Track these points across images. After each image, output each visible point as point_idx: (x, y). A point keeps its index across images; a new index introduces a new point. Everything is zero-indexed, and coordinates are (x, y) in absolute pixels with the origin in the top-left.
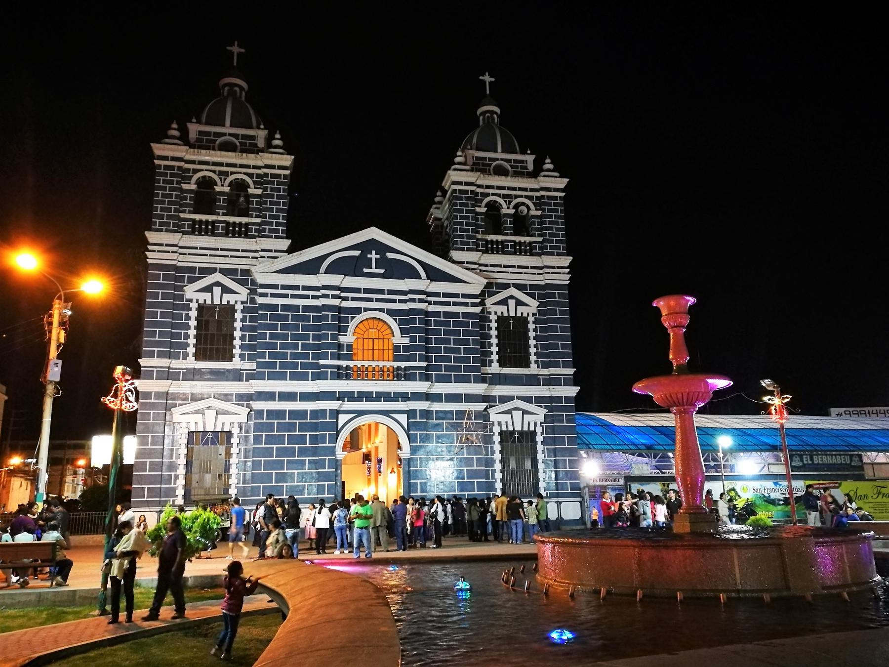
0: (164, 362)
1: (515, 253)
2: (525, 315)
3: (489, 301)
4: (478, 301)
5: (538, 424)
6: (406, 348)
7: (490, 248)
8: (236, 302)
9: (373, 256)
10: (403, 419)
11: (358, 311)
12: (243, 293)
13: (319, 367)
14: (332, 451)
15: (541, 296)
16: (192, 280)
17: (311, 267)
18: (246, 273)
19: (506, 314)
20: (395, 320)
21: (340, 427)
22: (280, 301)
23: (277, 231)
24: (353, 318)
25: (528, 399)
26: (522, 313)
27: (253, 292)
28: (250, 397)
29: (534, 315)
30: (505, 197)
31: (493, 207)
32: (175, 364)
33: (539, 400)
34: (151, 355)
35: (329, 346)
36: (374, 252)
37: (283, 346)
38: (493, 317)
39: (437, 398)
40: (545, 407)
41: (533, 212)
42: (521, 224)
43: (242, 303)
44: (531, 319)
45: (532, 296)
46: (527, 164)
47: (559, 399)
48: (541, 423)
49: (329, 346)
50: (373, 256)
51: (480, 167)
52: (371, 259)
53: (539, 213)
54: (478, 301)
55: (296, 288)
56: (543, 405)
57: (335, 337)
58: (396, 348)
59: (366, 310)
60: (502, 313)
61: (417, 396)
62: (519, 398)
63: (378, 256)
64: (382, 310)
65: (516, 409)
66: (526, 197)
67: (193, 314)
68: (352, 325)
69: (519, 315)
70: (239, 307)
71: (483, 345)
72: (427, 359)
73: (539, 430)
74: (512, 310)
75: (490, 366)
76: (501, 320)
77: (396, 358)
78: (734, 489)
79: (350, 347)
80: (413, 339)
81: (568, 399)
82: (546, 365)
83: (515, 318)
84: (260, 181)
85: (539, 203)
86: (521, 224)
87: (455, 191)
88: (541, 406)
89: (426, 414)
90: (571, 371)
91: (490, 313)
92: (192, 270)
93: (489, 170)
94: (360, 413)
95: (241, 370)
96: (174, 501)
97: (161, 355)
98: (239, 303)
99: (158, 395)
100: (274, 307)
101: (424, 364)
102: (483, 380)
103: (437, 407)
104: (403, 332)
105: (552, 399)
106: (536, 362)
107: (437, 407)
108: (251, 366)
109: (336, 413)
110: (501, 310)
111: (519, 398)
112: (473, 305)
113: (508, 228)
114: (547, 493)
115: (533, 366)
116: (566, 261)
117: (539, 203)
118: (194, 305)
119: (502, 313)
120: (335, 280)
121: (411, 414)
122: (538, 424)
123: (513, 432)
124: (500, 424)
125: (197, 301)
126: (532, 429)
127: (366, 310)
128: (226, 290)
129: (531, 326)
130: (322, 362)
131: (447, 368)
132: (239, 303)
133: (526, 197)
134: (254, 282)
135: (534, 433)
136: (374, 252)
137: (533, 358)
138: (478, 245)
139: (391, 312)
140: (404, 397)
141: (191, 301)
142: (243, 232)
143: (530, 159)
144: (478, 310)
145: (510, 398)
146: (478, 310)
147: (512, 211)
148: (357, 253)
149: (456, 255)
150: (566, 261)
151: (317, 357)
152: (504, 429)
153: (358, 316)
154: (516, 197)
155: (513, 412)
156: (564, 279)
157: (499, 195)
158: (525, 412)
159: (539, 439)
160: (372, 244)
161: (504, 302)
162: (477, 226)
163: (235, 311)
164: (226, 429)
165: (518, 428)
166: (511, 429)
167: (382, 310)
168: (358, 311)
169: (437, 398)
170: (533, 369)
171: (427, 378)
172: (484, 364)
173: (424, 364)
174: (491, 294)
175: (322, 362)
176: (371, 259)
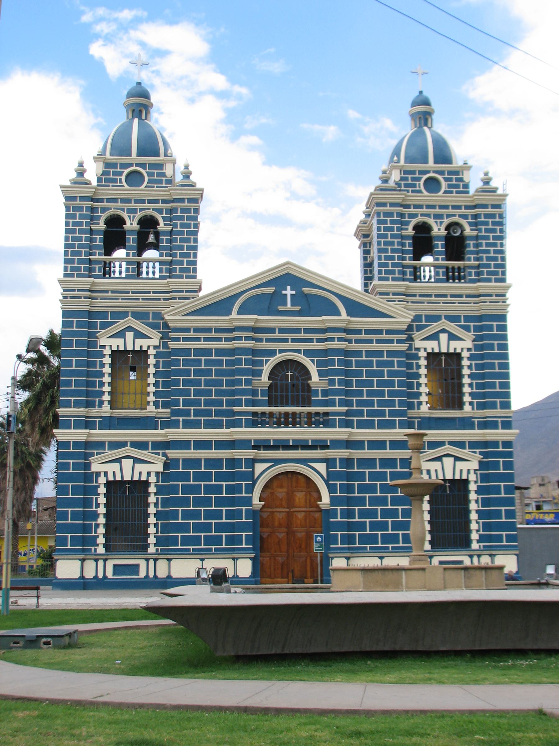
0: (82, 411)
1: (447, 280)
2: (458, 351)
4: (404, 337)
5: (472, 472)
8: (149, 347)
9: (289, 292)
10: (322, 468)
11: (272, 353)
13: (234, 413)
14: (248, 501)
15: (476, 329)
16: (105, 326)
18: (158, 315)
19: (437, 351)
20: (313, 361)
21: (256, 476)
22: (213, 345)
23: (393, 272)
24: (267, 361)
25: (460, 444)
26: (455, 349)
27: (165, 336)
28: (159, 446)
30: (437, 216)
32: (94, 412)
33: (474, 445)
34: (67, 404)
35: (243, 392)
36: (289, 288)
37: (218, 393)
40: (480, 453)
43: (155, 347)
45: (467, 328)
46: (462, 175)
47: (495, 444)
48: (475, 470)
49: (243, 392)
50: (289, 292)
52: (286, 295)
54: (404, 337)
55: (297, 331)
56: (161, 451)
57: (248, 382)
59: (281, 351)
60: (433, 349)
61: (337, 444)
62: (451, 443)
63: (294, 292)
64: (298, 351)
65: (448, 455)
66: (461, 216)
69: (451, 351)
71: (410, 386)
72: (348, 403)
73: (472, 477)
75: (419, 408)
76: (432, 357)
80: (332, 382)
82: (482, 406)
83: (448, 355)
88: (475, 452)
89: (348, 462)
92: (103, 315)
93: (121, 179)
94: (277, 462)
95: (156, 418)
96: (95, 550)
97: (77, 404)
98: (152, 348)
99: (77, 444)
102: (410, 425)
103: (357, 454)
105: (485, 444)
106: (471, 403)
107: (357, 454)
108: (164, 412)
109: (252, 462)
111: (451, 443)
112: (399, 341)
114: (480, 546)
115: (467, 408)
118: (422, 354)
119: (433, 349)
120: (250, 319)
121: (330, 462)
122: (472, 472)
123: (123, 482)
124: (106, 473)
125: (111, 346)
126: (464, 477)
127: (281, 351)
129: (152, 361)
130: (236, 409)
132: (152, 348)
133: (461, 216)
134: (166, 326)
135: (466, 482)
136: (289, 288)
137: (467, 399)
138: (404, 273)
139: (308, 353)
145: (441, 444)
146: (403, 347)
148: (271, 289)
151: (230, 403)
152: (111, 478)
153: (272, 359)
154: (448, 216)
155: (444, 459)
157: (428, 215)
158: (457, 459)
159: (472, 487)
161: (434, 337)
162: (403, 252)
163: (148, 356)
164: (144, 478)
165: (127, 478)
166: (119, 478)
167: (298, 351)
168: (272, 353)
171: (348, 424)
172: (411, 406)
174: (420, 328)
175: (236, 409)
176: (286, 295)
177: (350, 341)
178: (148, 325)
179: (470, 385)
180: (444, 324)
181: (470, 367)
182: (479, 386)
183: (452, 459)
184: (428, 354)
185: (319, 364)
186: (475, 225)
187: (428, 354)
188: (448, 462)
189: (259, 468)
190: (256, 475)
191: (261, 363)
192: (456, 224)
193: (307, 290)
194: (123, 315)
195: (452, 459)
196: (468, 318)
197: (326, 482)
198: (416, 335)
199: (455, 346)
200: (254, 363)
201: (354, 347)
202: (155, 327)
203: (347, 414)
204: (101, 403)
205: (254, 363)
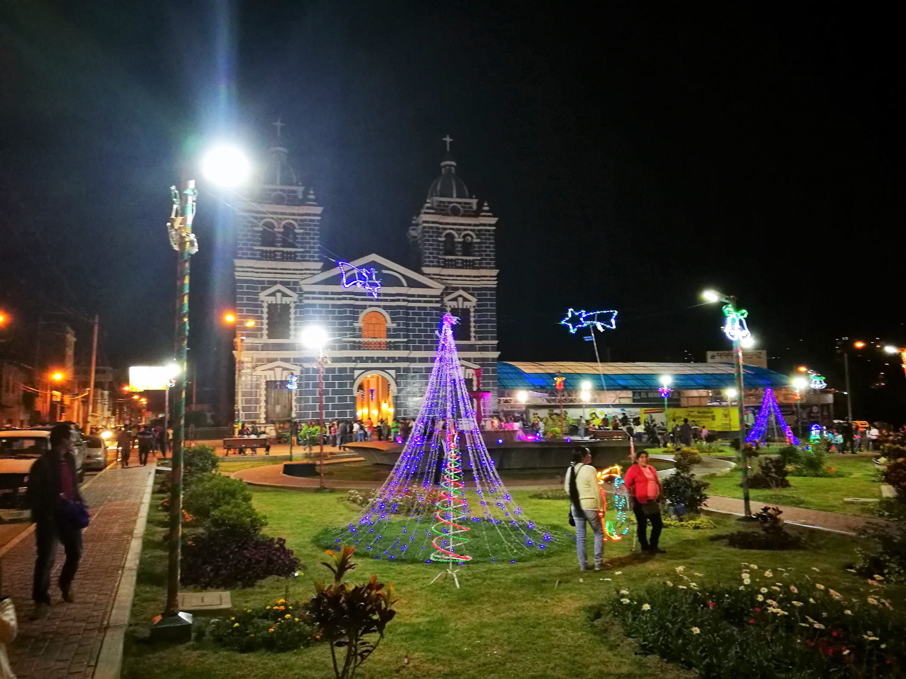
3: (446, 299)
6: (395, 330)
7: (448, 264)
10: (393, 372)
11: (365, 307)
12: (295, 296)
16: (264, 289)
17: (336, 280)
19: (274, 302)
29: (295, 302)
31: (450, 237)
38: (449, 309)
39: (413, 360)
41: (475, 240)
42: (467, 248)
44: (472, 310)
47: (487, 359)
51: (441, 210)
53: (478, 240)
58: (388, 330)
61: (401, 360)
64: (379, 306)
65: (277, 367)
67: (265, 310)
68: (361, 316)
69: (284, 303)
70: (292, 305)
72: (406, 336)
74: (279, 299)
76: (270, 306)
77: (389, 336)
78: (594, 413)
79: (360, 329)
80: (399, 325)
81: (493, 359)
82: (480, 339)
83: (281, 304)
84: (302, 224)
85: (479, 234)
86: (467, 248)
87: (425, 227)
90: (496, 342)
91: (446, 306)
92: (262, 282)
100: (425, 308)
101: (405, 340)
103: (413, 365)
104: (393, 320)
106: (475, 337)
109: (353, 370)
110: (271, 300)
112: (437, 302)
113: (459, 251)
115: (473, 339)
116: (495, 272)
117: (479, 234)
118: (265, 305)
121: (398, 370)
128: (465, 300)
129: (472, 314)
131: (420, 342)
133: (471, 230)
137: (473, 334)
139: (385, 308)
140: (393, 360)
141: (262, 302)
142: (287, 257)
143: (474, 202)
144: (439, 305)
146: (439, 305)
147: (461, 240)
149: (426, 270)
150: (495, 272)
156: (493, 284)
160: (374, 264)
161: (455, 299)
163: (290, 308)
167: (379, 306)
168: (365, 307)
169: (413, 360)
170: (473, 341)
171: (407, 348)
173: (405, 340)
177: (409, 301)
178: (289, 288)
179: (475, 327)
180: (461, 292)
181: (474, 317)
182: (480, 327)
183: (281, 369)
184: (269, 304)
185: (391, 314)
186: (478, 236)
187: (269, 304)
188: (278, 370)
189: (357, 373)
190: (355, 377)
191: (357, 313)
192: (468, 235)
193: (384, 272)
194: (275, 283)
195: (281, 369)
196: (474, 289)
197: (395, 380)
198: (446, 299)
199: (286, 300)
200: (354, 313)
201: (411, 305)
202: (294, 290)
203: (407, 342)
204: (262, 336)
205: (354, 313)
